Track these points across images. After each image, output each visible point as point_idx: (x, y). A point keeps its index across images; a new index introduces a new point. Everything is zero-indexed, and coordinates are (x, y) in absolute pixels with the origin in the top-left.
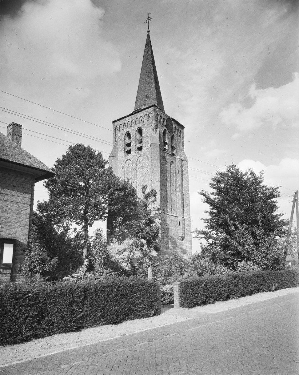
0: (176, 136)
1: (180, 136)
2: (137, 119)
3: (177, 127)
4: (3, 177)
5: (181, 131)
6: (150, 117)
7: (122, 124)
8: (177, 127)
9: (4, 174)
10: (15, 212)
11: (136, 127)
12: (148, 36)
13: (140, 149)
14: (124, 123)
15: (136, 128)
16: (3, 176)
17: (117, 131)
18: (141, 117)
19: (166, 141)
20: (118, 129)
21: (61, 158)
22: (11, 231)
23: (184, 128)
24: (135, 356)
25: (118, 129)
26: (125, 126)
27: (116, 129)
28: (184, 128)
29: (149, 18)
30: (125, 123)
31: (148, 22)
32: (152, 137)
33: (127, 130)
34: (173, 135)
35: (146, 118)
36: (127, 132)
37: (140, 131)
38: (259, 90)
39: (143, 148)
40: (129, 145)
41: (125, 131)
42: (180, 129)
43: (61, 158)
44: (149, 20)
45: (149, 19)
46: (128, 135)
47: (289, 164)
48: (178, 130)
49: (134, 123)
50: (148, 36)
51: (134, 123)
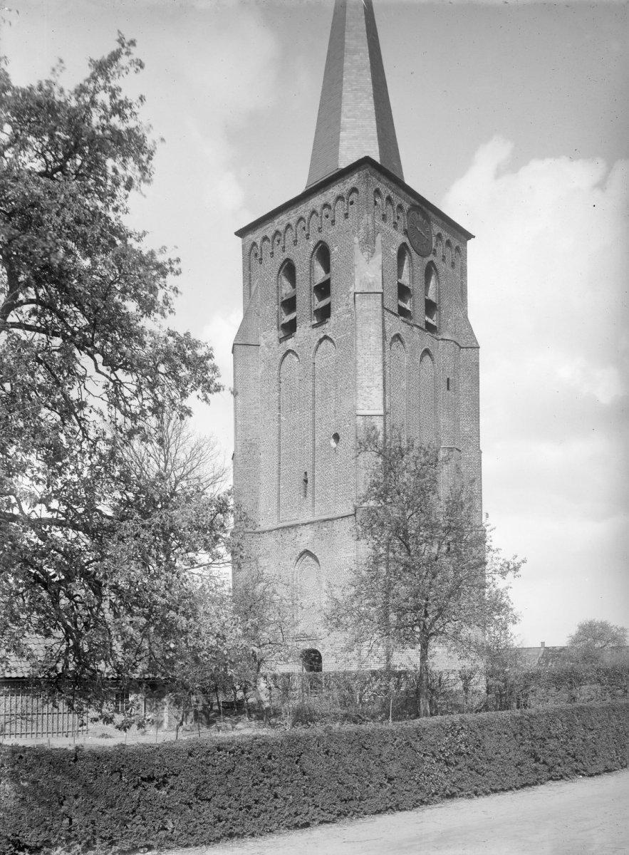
0: (442, 267)
1: (453, 265)
3: (444, 234)
5: (457, 249)
6: (352, 203)
8: (444, 234)
11: (312, 243)
13: (324, 314)
14: (273, 232)
17: (255, 262)
20: (256, 255)
23: (469, 236)
24: (153, 728)
25: (256, 255)
26: (279, 241)
28: (469, 236)
32: (366, 272)
33: (286, 255)
34: (431, 263)
36: (284, 262)
37: (323, 253)
39: (332, 307)
40: (290, 304)
41: (280, 258)
42: (455, 243)
43: (115, 51)
46: (289, 269)
48: (448, 243)
49: (304, 228)
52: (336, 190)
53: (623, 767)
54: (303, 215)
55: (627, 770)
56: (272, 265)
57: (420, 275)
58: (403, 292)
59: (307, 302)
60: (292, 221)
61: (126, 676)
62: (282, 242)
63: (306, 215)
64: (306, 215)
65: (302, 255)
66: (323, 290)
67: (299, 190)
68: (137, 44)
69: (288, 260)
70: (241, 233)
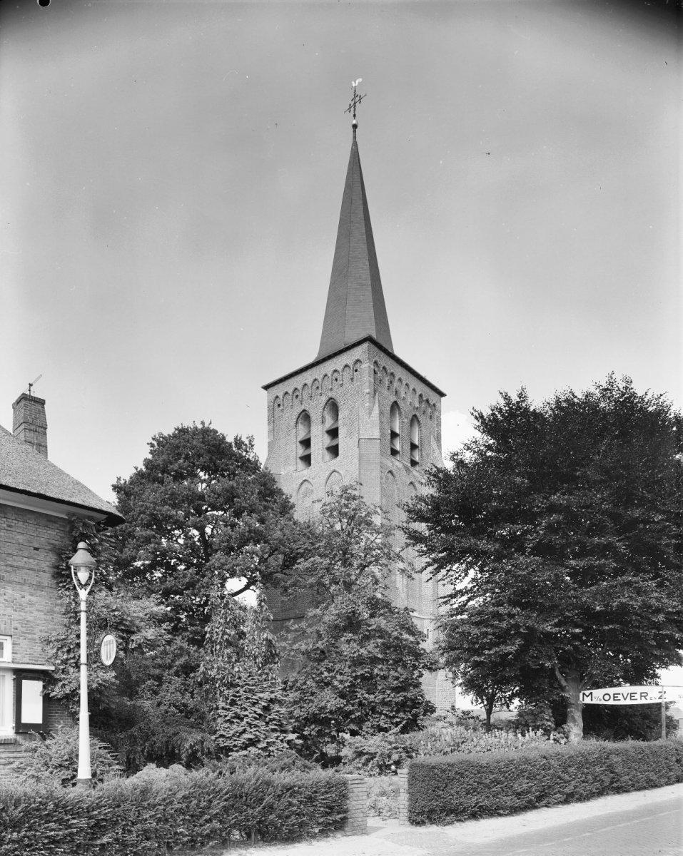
2: (326, 377)
4: (9, 529)
6: (356, 371)
7: (290, 392)
9: (10, 520)
10: (41, 608)
12: (355, 144)
14: (293, 389)
15: (324, 399)
16: (9, 526)
18: (335, 371)
19: (397, 431)
21: (142, 467)
22: (35, 652)
27: (276, 405)
29: (355, 96)
30: (296, 389)
31: (352, 109)
33: (303, 408)
35: (347, 375)
37: (333, 406)
38: (589, 739)
40: (306, 443)
43: (142, 467)
44: (355, 103)
45: (357, 99)
46: (305, 417)
47: (670, 676)
49: (318, 387)
50: (355, 144)
51: (318, 387)
52: (338, 363)
53: (678, 782)
54: (306, 382)
55: (681, 785)
56: (292, 413)
57: (407, 426)
58: (394, 435)
59: (320, 442)
60: (309, 382)
61: (217, 685)
62: (300, 397)
63: (340, 368)
64: (340, 368)
65: (316, 408)
66: (334, 433)
67: (311, 359)
68: (111, 488)
69: (304, 411)
70: (266, 387)
